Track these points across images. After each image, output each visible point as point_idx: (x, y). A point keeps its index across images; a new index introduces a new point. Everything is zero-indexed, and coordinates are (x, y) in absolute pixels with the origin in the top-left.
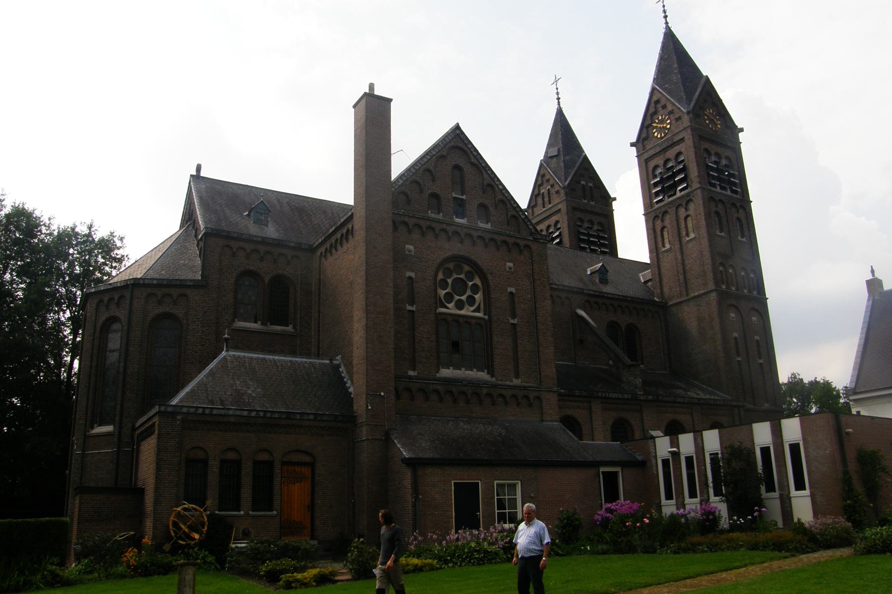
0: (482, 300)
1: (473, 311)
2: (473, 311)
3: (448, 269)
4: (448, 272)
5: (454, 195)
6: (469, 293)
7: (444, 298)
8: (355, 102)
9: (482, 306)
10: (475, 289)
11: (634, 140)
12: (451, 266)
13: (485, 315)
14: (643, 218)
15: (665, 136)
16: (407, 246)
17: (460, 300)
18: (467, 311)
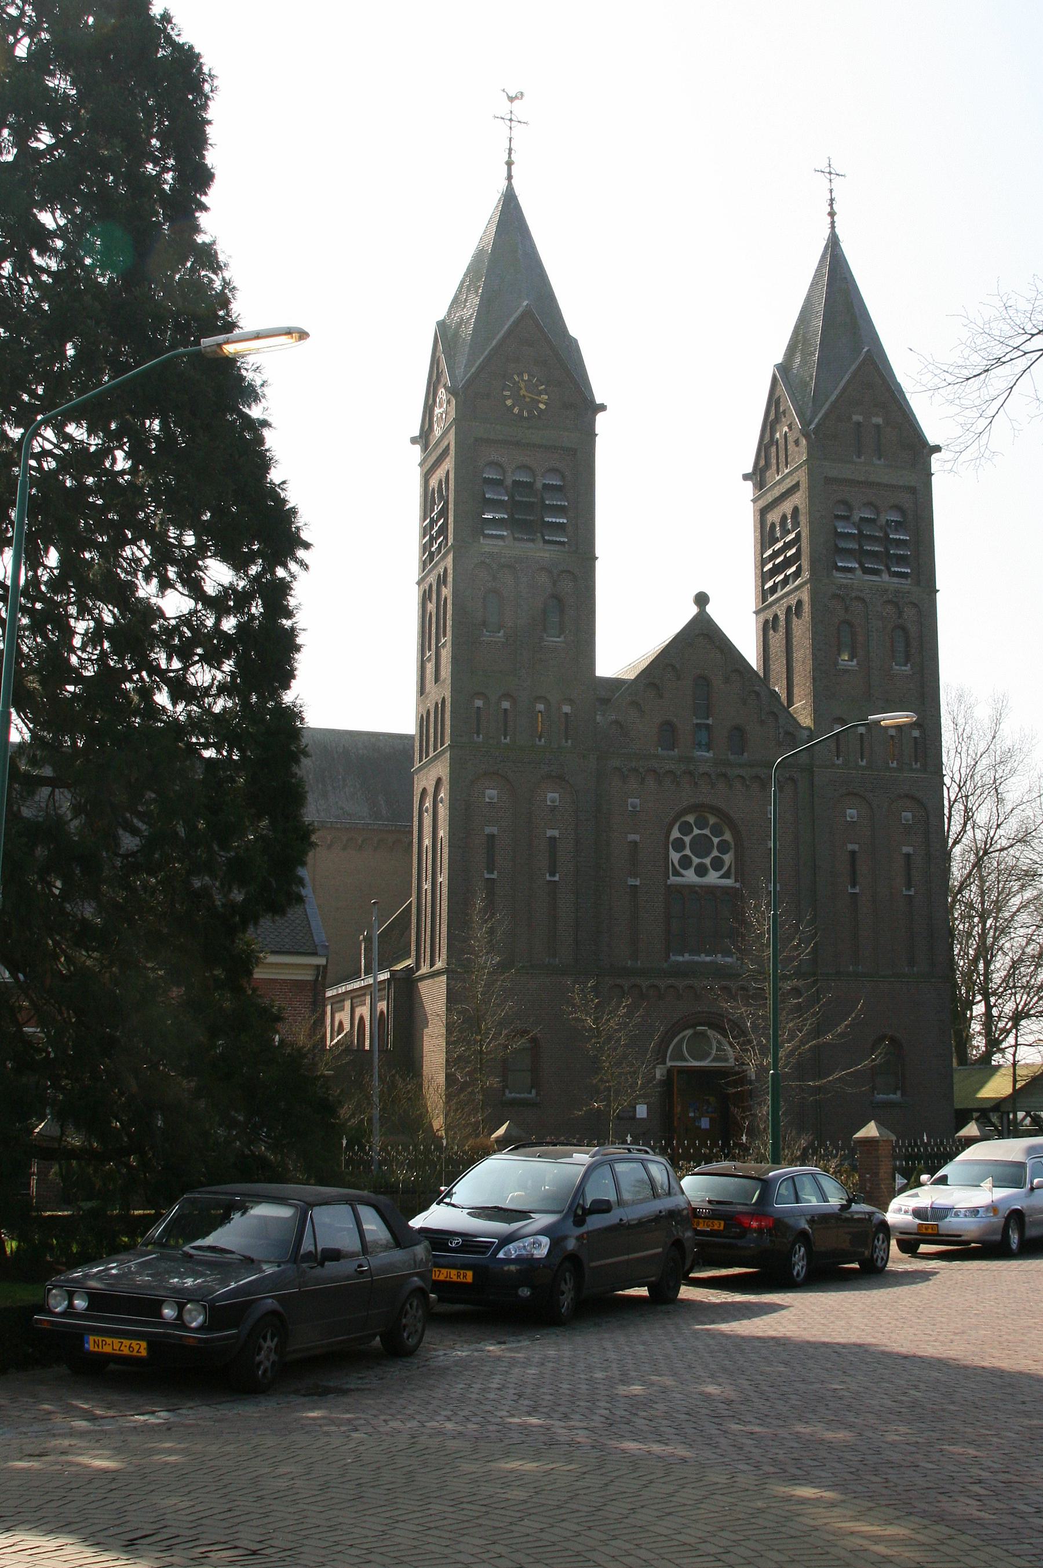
0: (733, 864)
1: (721, 877)
2: (721, 877)
3: (687, 823)
4: (701, 824)
5: (696, 721)
6: (715, 853)
7: (679, 865)
8: (420, 421)
9: (733, 870)
10: (723, 847)
11: (749, 469)
12: (691, 819)
13: (736, 881)
14: (598, 552)
15: (1009, 1129)
16: (904, 814)
17: (713, 859)
18: (713, 878)
